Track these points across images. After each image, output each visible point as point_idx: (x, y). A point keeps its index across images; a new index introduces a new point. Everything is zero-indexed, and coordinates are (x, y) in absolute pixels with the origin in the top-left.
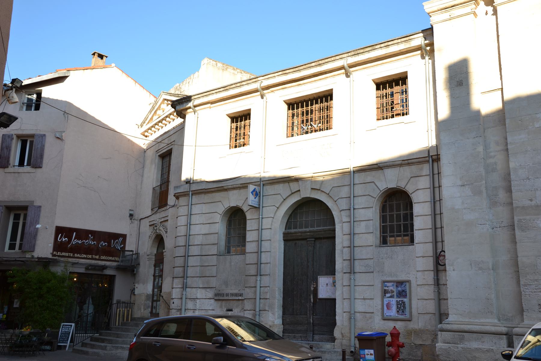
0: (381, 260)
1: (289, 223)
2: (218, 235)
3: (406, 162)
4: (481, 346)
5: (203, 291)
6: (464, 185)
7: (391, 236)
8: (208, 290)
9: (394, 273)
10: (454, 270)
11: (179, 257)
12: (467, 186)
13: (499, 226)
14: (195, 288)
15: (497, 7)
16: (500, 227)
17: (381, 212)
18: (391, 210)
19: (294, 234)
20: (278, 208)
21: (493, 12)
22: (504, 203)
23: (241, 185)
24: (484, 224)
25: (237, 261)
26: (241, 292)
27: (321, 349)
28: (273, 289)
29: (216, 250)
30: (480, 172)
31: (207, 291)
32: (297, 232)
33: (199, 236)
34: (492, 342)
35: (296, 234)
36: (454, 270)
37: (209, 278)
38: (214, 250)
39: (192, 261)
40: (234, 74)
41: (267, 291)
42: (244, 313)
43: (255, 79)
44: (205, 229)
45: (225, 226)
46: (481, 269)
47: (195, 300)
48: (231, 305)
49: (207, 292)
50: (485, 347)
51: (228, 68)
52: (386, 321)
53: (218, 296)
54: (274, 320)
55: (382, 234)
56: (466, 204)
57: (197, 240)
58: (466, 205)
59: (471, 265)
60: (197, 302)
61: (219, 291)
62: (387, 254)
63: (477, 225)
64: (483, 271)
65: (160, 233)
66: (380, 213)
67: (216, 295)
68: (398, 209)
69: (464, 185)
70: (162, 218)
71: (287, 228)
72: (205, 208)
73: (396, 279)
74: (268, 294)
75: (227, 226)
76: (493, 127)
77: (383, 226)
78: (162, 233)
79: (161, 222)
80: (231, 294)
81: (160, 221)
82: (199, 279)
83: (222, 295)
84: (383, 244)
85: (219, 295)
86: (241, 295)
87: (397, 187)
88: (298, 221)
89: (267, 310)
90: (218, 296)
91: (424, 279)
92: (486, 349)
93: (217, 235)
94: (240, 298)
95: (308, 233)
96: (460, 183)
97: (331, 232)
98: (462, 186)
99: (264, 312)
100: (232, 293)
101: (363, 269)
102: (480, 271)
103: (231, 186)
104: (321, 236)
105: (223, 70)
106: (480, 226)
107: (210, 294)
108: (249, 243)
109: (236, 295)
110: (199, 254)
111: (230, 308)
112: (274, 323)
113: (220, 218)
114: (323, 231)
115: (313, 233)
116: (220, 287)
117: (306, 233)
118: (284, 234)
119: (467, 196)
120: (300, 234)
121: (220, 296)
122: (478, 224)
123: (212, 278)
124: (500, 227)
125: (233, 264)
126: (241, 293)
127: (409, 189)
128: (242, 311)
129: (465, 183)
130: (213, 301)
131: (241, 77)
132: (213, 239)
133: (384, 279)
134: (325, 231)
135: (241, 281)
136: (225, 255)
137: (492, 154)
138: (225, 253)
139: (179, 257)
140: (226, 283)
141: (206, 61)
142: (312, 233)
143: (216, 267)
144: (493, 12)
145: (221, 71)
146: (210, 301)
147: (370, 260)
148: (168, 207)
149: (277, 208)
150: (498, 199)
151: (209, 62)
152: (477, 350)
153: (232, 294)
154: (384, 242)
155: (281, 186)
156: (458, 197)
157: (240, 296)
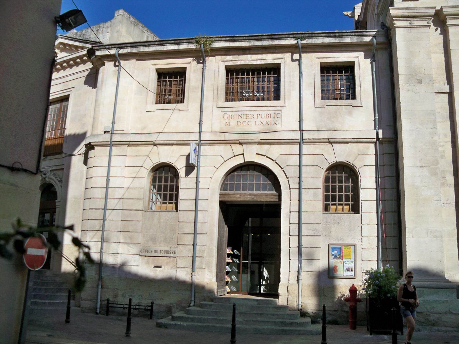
0: (328, 225)
1: (224, 184)
2: (144, 190)
3: (356, 140)
4: (437, 299)
5: (125, 246)
6: (422, 167)
7: (333, 205)
8: (131, 245)
9: (340, 237)
10: (412, 237)
11: (94, 209)
12: (425, 168)
13: (446, 203)
14: (115, 242)
15: (449, 27)
16: (446, 203)
17: (324, 182)
18: (334, 181)
19: (232, 196)
20: (217, 169)
21: (440, 32)
22: (450, 185)
23: (175, 142)
24: (438, 200)
25: (168, 218)
26: (173, 249)
27: (270, 306)
28: (210, 247)
29: (142, 205)
30: (436, 157)
31: (130, 247)
32: (236, 194)
33: (120, 190)
34: (446, 295)
35: (235, 196)
36: (412, 237)
37: (133, 233)
38: (140, 205)
39: (110, 215)
40: (142, 31)
41: (204, 250)
42: (176, 270)
43: (161, 43)
44: (127, 183)
45: (149, 182)
46: (435, 236)
47: (115, 255)
48: (160, 261)
49: (130, 248)
50: (441, 299)
51: (138, 24)
52: (330, 279)
53: (144, 252)
54: (212, 278)
55: (324, 202)
56: (424, 182)
57: (118, 194)
58: (424, 183)
59: (427, 233)
60: (117, 257)
61: (146, 247)
62: (334, 220)
63: (433, 201)
64: (437, 238)
65: (50, 182)
66: (323, 183)
67: (142, 251)
68: (340, 181)
69: (422, 167)
70: (54, 166)
71: (222, 189)
72: (128, 161)
73: (342, 243)
74: (206, 252)
75: (150, 181)
76: (442, 122)
77: (326, 195)
78: (53, 182)
79: (51, 171)
80: (160, 251)
81: (50, 169)
82: (120, 234)
83: (150, 251)
84: (325, 211)
85: (145, 251)
86: (174, 252)
87: (345, 162)
88: (235, 183)
89: (204, 268)
90: (144, 252)
91: (369, 243)
92: (442, 301)
93: (142, 190)
94: (172, 255)
95: (249, 196)
96: (419, 164)
97: (272, 196)
98: (421, 167)
99: (200, 270)
100: (162, 250)
101: (311, 233)
102: (434, 238)
103: (163, 141)
104: (263, 200)
105: (134, 25)
106: (435, 201)
107: (134, 249)
108: (183, 201)
109: (167, 252)
110: (121, 208)
111: (159, 265)
112: (211, 280)
113: (147, 173)
114: (265, 195)
115: (254, 196)
116: (146, 243)
117: (246, 196)
118: (220, 195)
119: (425, 176)
120: (239, 196)
121: (146, 252)
122: (434, 200)
123: (136, 234)
124: (446, 203)
125: (162, 221)
126: (174, 250)
127: (357, 164)
128: (174, 269)
129: (424, 165)
130: (138, 257)
131: (147, 36)
132: (135, 194)
133: (331, 243)
134: (267, 195)
135: (173, 238)
136: (148, 210)
137: (441, 144)
138: (149, 209)
139: (94, 209)
140: (154, 240)
141: (121, 12)
142: (252, 196)
143: (141, 222)
144: (440, 32)
145: (133, 25)
146: (134, 257)
147: (318, 225)
148: (63, 155)
149: (216, 169)
150: (445, 180)
151: (124, 14)
152: (435, 301)
153: (163, 251)
154: (326, 209)
155: (222, 147)
156: (418, 176)
157: (173, 253)
